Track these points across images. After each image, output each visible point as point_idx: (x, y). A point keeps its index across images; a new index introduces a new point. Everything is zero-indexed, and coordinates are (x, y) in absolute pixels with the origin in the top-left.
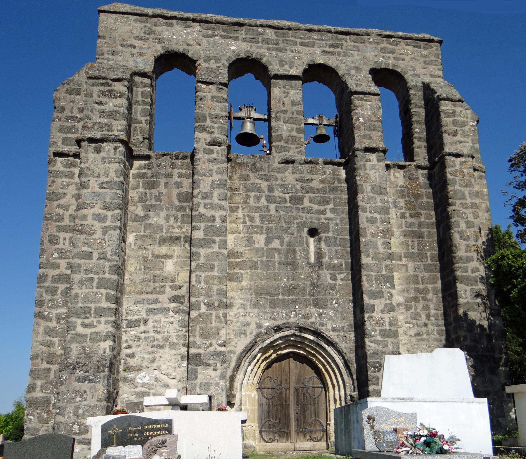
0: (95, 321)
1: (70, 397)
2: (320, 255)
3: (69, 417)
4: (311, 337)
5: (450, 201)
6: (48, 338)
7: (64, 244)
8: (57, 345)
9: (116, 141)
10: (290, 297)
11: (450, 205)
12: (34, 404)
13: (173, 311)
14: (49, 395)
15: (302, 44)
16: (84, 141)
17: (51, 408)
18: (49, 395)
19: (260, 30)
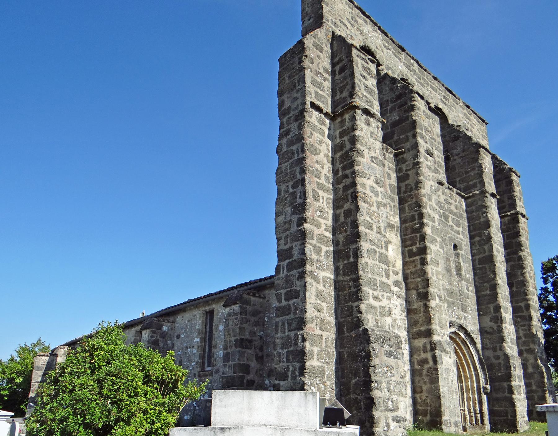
0: (380, 294)
1: (383, 371)
2: (458, 268)
3: (385, 393)
4: (463, 336)
5: (522, 248)
6: (319, 302)
7: (323, 203)
8: (325, 311)
9: (379, 121)
10: (451, 299)
11: (521, 250)
12: (313, 373)
13: (396, 295)
14: (323, 365)
15: (431, 87)
16: (360, 109)
17: (326, 379)
18: (323, 365)
19: (412, 61)
